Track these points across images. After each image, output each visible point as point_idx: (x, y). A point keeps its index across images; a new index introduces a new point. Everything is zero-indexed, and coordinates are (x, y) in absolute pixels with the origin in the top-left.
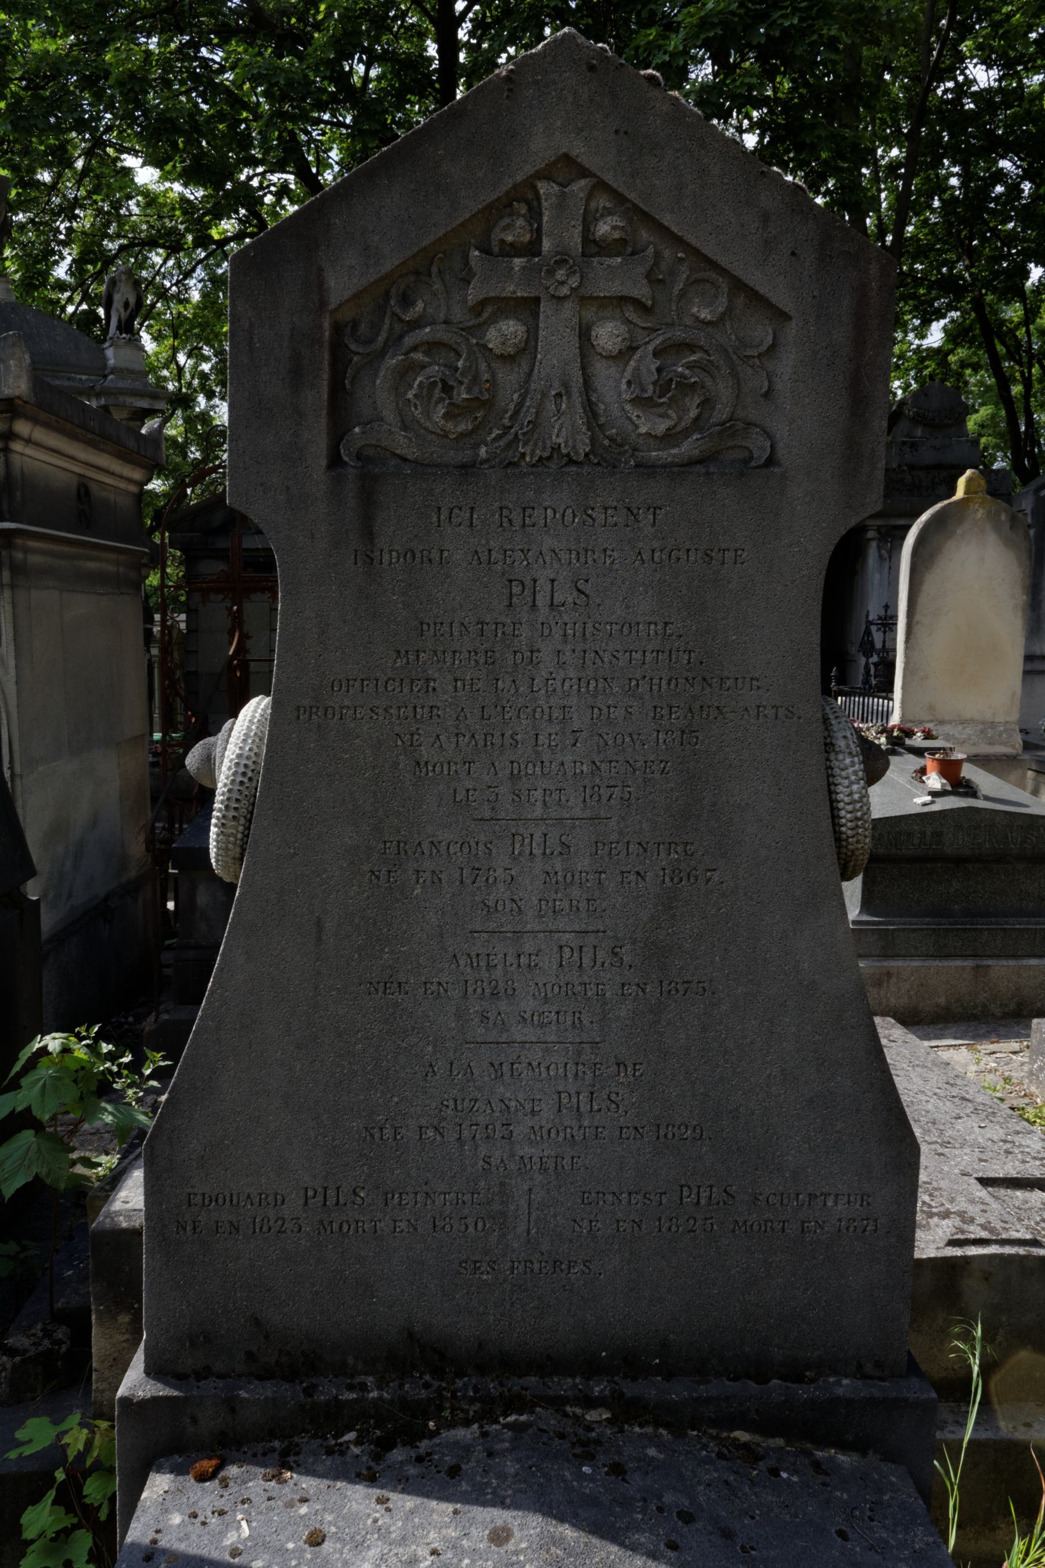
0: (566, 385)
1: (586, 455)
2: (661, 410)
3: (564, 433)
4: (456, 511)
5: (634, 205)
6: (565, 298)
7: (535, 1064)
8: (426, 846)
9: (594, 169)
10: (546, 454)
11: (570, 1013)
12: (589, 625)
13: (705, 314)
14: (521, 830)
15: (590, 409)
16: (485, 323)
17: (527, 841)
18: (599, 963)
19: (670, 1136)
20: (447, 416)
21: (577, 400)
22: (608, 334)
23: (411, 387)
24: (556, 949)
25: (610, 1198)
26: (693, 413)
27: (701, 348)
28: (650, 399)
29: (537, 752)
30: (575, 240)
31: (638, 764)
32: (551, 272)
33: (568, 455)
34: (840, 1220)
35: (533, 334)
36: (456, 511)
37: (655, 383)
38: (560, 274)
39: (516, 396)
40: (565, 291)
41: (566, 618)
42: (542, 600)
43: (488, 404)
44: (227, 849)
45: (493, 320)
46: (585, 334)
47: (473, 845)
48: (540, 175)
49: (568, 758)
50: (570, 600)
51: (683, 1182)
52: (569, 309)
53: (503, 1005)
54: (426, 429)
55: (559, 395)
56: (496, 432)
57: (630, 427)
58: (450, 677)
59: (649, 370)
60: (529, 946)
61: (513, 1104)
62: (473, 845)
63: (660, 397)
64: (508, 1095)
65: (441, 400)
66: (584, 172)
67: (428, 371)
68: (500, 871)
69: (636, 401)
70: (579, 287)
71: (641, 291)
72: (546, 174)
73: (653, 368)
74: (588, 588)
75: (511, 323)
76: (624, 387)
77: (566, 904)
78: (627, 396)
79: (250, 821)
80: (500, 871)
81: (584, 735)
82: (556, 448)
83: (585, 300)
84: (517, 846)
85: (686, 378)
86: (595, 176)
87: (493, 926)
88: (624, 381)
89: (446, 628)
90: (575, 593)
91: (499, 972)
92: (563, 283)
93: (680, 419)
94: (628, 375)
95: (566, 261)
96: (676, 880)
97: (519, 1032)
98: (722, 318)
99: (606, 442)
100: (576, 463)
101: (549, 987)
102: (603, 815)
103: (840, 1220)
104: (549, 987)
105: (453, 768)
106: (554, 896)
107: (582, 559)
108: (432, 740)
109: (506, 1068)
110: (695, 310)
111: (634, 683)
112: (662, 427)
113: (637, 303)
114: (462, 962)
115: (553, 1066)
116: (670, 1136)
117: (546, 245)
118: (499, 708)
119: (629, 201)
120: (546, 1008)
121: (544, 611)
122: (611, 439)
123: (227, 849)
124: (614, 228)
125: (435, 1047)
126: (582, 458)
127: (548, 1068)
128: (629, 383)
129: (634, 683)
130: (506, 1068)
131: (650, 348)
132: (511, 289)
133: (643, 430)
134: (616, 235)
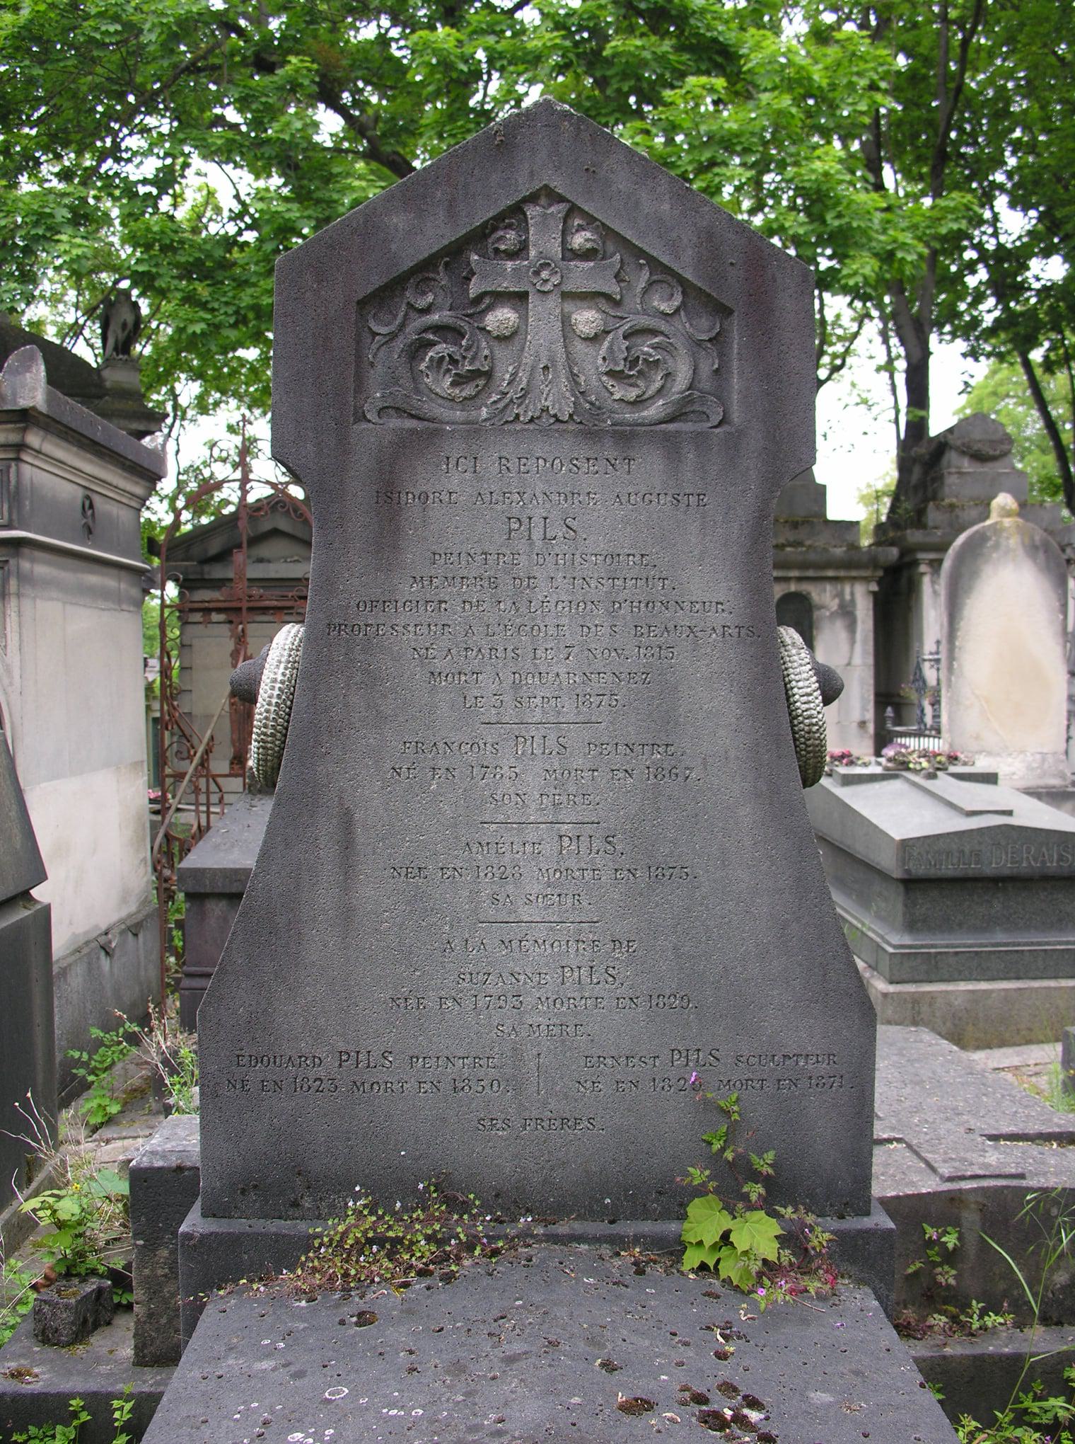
0: (552, 359)
1: (571, 416)
2: (632, 381)
3: (551, 398)
4: (462, 460)
5: (603, 224)
6: (549, 292)
7: (540, 941)
8: (441, 745)
9: (568, 196)
10: (537, 414)
11: (570, 896)
12: (577, 556)
13: (664, 307)
14: (524, 733)
15: (573, 377)
16: (483, 311)
17: (529, 742)
18: (594, 851)
19: (661, 1005)
20: (453, 384)
21: (563, 373)
22: (586, 319)
23: (423, 359)
24: (557, 838)
25: (609, 1061)
26: (658, 385)
27: (662, 333)
28: (622, 371)
29: (535, 665)
30: (556, 250)
31: (623, 676)
32: (537, 273)
33: (555, 416)
34: (810, 1078)
35: (524, 318)
36: (462, 460)
37: (625, 359)
38: (544, 274)
39: (510, 369)
40: (548, 287)
41: (557, 550)
42: (537, 535)
43: (489, 375)
44: (266, 760)
45: (490, 308)
46: (566, 321)
47: (482, 746)
48: (526, 200)
49: (562, 670)
50: (560, 534)
51: (673, 1047)
52: (553, 302)
53: (510, 889)
54: (437, 394)
55: (546, 368)
56: (495, 397)
57: (607, 395)
58: (459, 600)
59: (620, 349)
60: (532, 836)
61: (522, 977)
62: (482, 746)
63: (630, 369)
64: (517, 969)
65: (448, 370)
66: (561, 199)
67: (438, 348)
68: (506, 768)
69: (610, 373)
70: (559, 284)
71: (613, 289)
72: (533, 198)
73: (623, 347)
74: (574, 524)
75: (506, 311)
76: (600, 361)
77: (564, 798)
78: (603, 369)
79: (285, 736)
80: (506, 768)
81: (575, 650)
82: (545, 410)
83: (566, 296)
84: (520, 747)
85: (651, 355)
86: (568, 201)
87: (501, 818)
88: (600, 358)
89: (454, 558)
90: (565, 529)
91: (506, 859)
92: (546, 281)
93: (647, 387)
94: (603, 352)
95: (549, 265)
96: (659, 777)
97: (525, 913)
98: (677, 311)
99: (587, 406)
100: (562, 422)
101: (551, 871)
102: (593, 719)
103: (810, 1078)
104: (551, 871)
105: (463, 678)
106: (554, 791)
107: (570, 501)
108: (444, 653)
109: (515, 944)
110: (656, 303)
111: (617, 605)
112: (632, 394)
113: (607, 297)
114: (474, 850)
115: (556, 944)
116: (661, 1005)
117: (533, 253)
118: (502, 627)
119: (596, 220)
120: (549, 891)
121: (539, 543)
122: (591, 403)
123: (266, 760)
124: (587, 240)
125: (452, 926)
126: (566, 418)
127: (552, 945)
128: (604, 359)
129: (617, 605)
130: (515, 944)
131: (621, 332)
132: (507, 285)
133: (617, 397)
134: (589, 245)
